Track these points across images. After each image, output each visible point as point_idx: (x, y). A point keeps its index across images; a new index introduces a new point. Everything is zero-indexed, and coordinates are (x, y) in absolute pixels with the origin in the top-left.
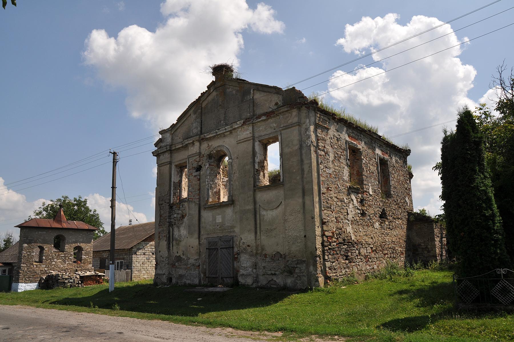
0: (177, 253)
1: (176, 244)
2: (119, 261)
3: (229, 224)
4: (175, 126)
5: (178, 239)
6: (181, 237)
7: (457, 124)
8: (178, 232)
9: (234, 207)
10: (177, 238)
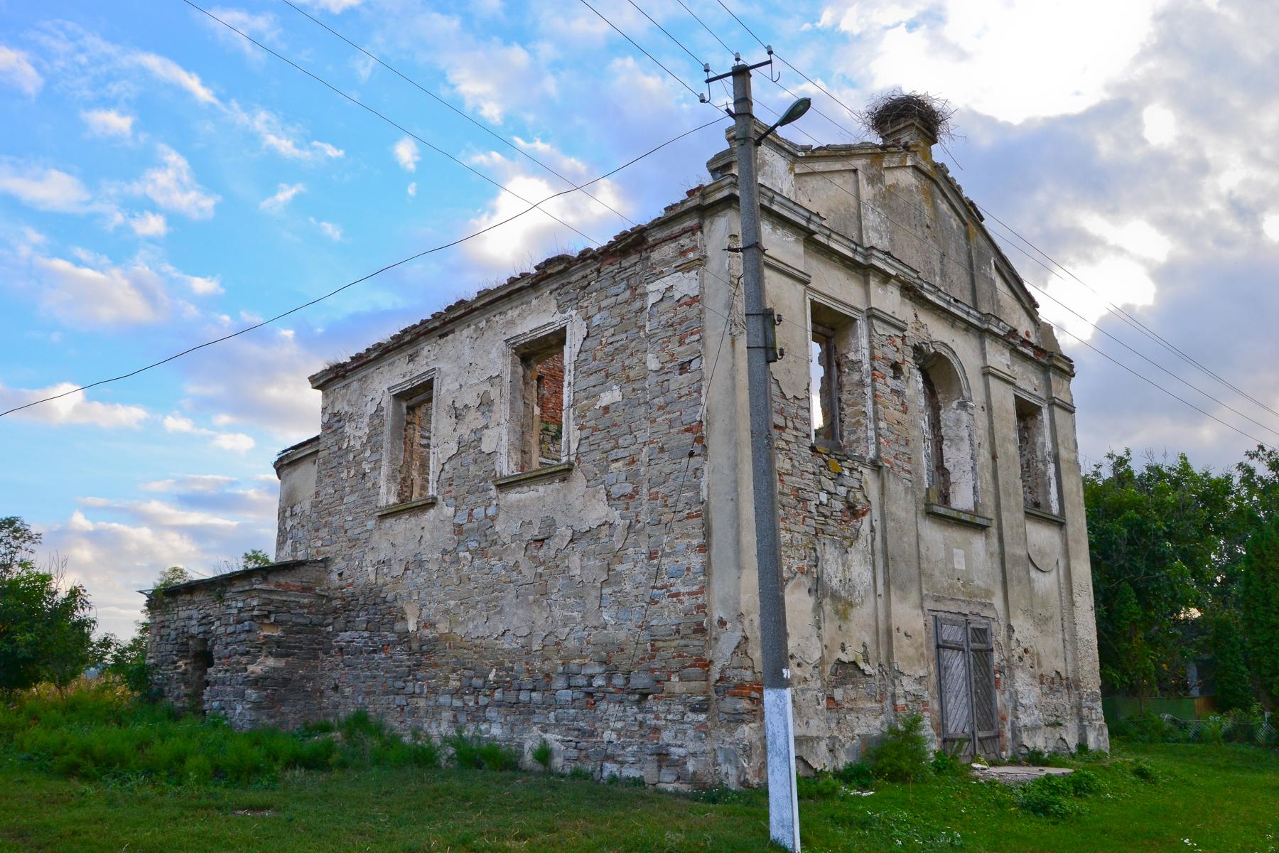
0: (843, 644)
1: (837, 612)
3: (981, 583)
4: (976, 222)
5: (843, 593)
6: (854, 591)
7: (1038, 310)
8: (841, 568)
9: (986, 538)
10: (836, 591)
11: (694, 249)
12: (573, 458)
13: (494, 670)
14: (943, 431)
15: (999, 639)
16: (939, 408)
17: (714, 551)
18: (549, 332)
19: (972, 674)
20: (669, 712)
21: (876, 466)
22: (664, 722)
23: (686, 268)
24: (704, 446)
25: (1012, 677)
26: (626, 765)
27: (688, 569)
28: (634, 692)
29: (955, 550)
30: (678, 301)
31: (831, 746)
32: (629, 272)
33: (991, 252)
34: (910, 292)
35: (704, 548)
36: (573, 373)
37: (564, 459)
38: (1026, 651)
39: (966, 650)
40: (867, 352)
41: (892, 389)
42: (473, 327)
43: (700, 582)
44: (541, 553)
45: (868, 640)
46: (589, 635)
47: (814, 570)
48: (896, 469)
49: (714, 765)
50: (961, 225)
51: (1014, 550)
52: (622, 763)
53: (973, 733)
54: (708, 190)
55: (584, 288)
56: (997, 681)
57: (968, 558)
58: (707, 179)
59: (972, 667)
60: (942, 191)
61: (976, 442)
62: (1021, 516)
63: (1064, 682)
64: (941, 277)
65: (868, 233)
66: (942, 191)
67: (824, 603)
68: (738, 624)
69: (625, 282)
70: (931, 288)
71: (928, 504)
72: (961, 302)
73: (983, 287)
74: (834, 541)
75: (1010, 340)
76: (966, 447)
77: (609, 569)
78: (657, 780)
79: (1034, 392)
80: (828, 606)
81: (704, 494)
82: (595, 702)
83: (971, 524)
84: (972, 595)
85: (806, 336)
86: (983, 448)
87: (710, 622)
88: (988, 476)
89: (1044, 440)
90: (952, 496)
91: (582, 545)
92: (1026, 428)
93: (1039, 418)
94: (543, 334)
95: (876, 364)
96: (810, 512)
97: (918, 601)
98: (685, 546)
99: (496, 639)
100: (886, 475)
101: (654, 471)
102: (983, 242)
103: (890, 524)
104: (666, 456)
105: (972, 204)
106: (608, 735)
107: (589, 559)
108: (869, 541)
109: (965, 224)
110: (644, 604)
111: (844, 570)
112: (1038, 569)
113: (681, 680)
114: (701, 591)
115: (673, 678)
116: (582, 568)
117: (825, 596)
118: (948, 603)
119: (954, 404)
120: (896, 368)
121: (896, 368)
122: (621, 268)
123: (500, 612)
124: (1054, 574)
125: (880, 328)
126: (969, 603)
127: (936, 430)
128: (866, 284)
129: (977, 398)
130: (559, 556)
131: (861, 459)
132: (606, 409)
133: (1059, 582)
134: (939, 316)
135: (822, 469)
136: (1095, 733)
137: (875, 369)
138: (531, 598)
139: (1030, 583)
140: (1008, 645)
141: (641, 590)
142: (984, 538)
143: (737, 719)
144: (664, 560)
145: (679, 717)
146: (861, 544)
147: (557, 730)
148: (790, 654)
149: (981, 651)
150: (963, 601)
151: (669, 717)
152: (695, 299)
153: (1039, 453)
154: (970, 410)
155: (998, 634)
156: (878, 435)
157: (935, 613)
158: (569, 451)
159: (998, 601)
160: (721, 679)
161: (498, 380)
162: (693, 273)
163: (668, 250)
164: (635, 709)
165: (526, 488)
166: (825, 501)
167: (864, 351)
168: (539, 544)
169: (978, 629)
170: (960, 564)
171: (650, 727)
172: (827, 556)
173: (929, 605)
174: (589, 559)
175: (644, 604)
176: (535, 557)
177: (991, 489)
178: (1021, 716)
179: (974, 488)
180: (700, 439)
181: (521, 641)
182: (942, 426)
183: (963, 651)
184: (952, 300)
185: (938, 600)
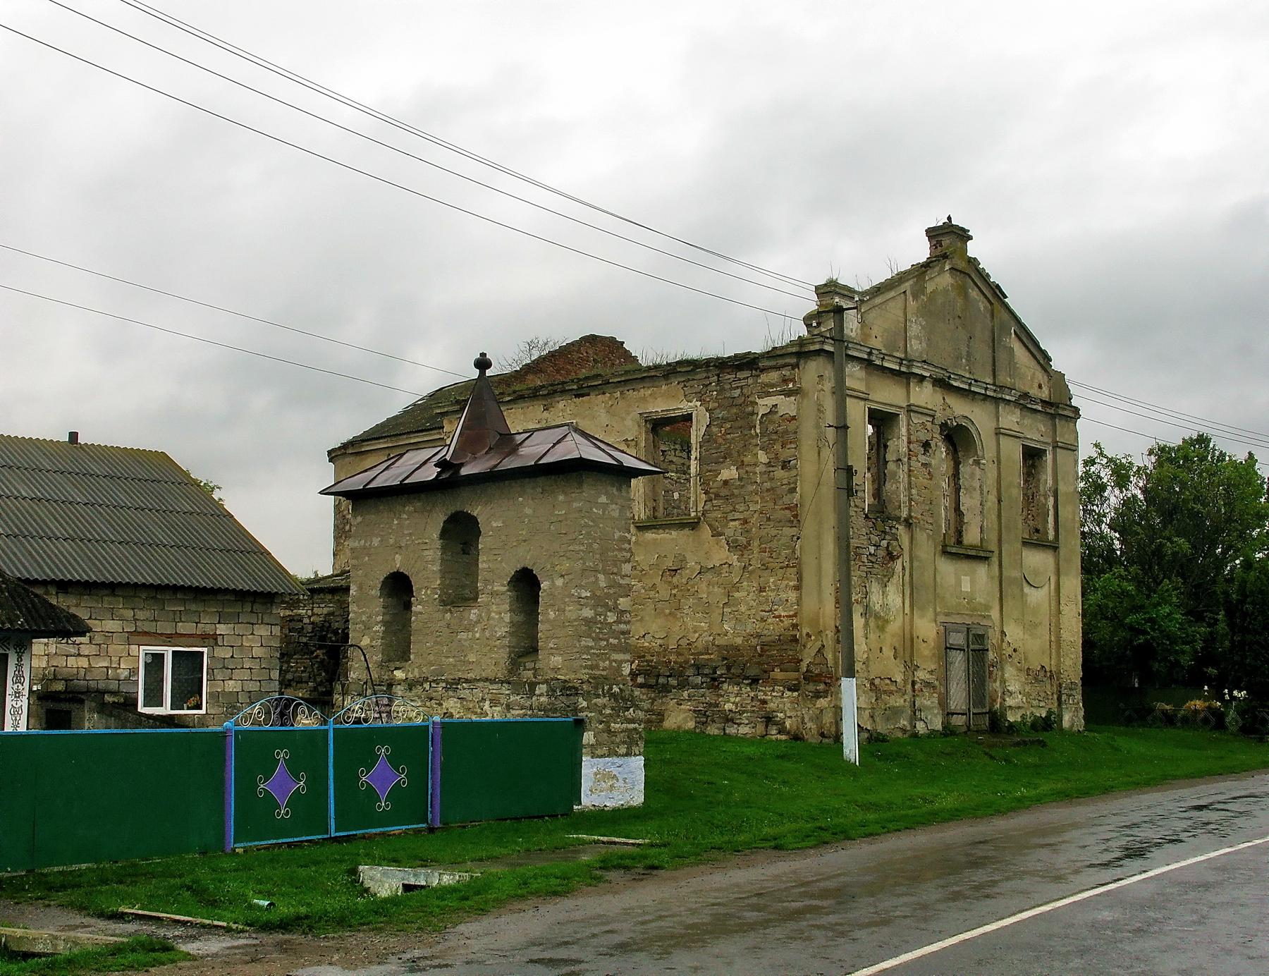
0: (881, 648)
2: (168, 651)
3: (982, 601)
6: (889, 612)
8: (881, 597)
9: (988, 565)
11: (793, 380)
12: (700, 514)
13: (637, 662)
14: (961, 481)
15: (994, 641)
16: (960, 463)
17: (804, 591)
18: (678, 414)
19: (971, 667)
20: (773, 691)
21: (908, 523)
22: (770, 698)
23: (789, 393)
24: (799, 520)
25: (1002, 669)
26: (742, 725)
27: (787, 600)
28: (747, 678)
29: (962, 577)
30: (782, 416)
31: (871, 714)
32: (743, 383)
33: (1013, 323)
34: (942, 384)
35: (798, 588)
36: (698, 450)
37: (693, 514)
38: (1015, 650)
39: (966, 650)
40: (905, 439)
41: (922, 464)
42: (608, 395)
43: (795, 609)
44: (675, 580)
45: (1006, 300)
46: (714, 639)
47: (864, 600)
48: (922, 522)
49: (802, 723)
50: (988, 305)
51: (1011, 573)
52: (739, 724)
53: (969, 709)
54: (805, 342)
55: (707, 386)
56: (991, 673)
57: (973, 582)
58: (804, 332)
59: (971, 663)
60: (973, 280)
61: (985, 490)
62: (1019, 545)
63: (1048, 674)
64: (966, 360)
65: (911, 342)
66: (973, 280)
67: (870, 621)
68: (820, 637)
69: (739, 390)
70: (956, 377)
71: (945, 546)
72: (980, 382)
73: (1002, 356)
74: (877, 579)
75: (1023, 402)
76: (977, 494)
77: (729, 596)
78: (765, 733)
79: (1042, 439)
80: (872, 623)
81: (798, 553)
82: (719, 684)
83: (978, 556)
84: (975, 609)
85: (865, 422)
86: (991, 495)
87: (801, 635)
88: (994, 517)
89: (1047, 478)
90: (964, 533)
91: (709, 576)
92: (1033, 466)
93: (1044, 458)
94: (673, 415)
95: (911, 446)
96: (863, 562)
97: (933, 617)
98: (785, 586)
99: (638, 639)
100: (914, 528)
101: (764, 533)
102: (1006, 316)
103: (916, 564)
104: (772, 524)
105: (998, 286)
106: (728, 706)
107: (713, 587)
108: (901, 577)
109: (991, 303)
110: (755, 620)
111: (883, 598)
112: (1028, 583)
113: (781, 671)
114: (795, 615)
115: (776, 670)
116: (709, 594)
117: (870, 616)
118: (954, 616)
119: (971, 461)
120: (926, 445)
121: (926, 445)
122: (736, 378)
123: (641, 620)
124: (1046, 587)
125: (916, 419)
126: (971, 616)
127: (956, 479)
128: (908, 384)
129: (989, 453)
130: (689, 583)
131: (898, 519)
132: (726, 482)
133: (1050, 593)
134: (963, 395)
135: (871, 529)
136: (1071, 714)
137: (910, 451)
138: (667, 611)
139: (1022, 598)
140: (1000, 648)
141: (753, 611)
142: (987, 566)
143: (817, 695)
144: (770, 593)
145: (780, 694)
146: (895, 580)
147: (689, 703)
148: (475, 374)
149: (979, 650)
150: (967, 615)
151: (774, 694)
152: (794, 418)
153: (1041, 488)
154: (982, 466)
155: (993, 638)
156: (911, 500)
157: (945, 624)
158: (697, 509)
159: (995, 614)
160: (807, 671)
161: (634, 443)
162: (793, 398)
163: (773, 376)
164: (749, 689)
165: (661, 531)
166: (873, 552)
167: (904, 438)
168: (673, 573)
169: (978, 635)
170: (966, 587)
171: (760, 700)
172: (873, 590)
173: (942, 618)
174: (713, 587)
175: (755, 620)
176: (670, 582)
177: (996, 527)
178: (1007, 699)
179: (981, 528)
180: (796, 516)
181: (659, 642)
182: (961, 477)
183: (964, 650)
184: (973, 382)
185: (947, 615)
